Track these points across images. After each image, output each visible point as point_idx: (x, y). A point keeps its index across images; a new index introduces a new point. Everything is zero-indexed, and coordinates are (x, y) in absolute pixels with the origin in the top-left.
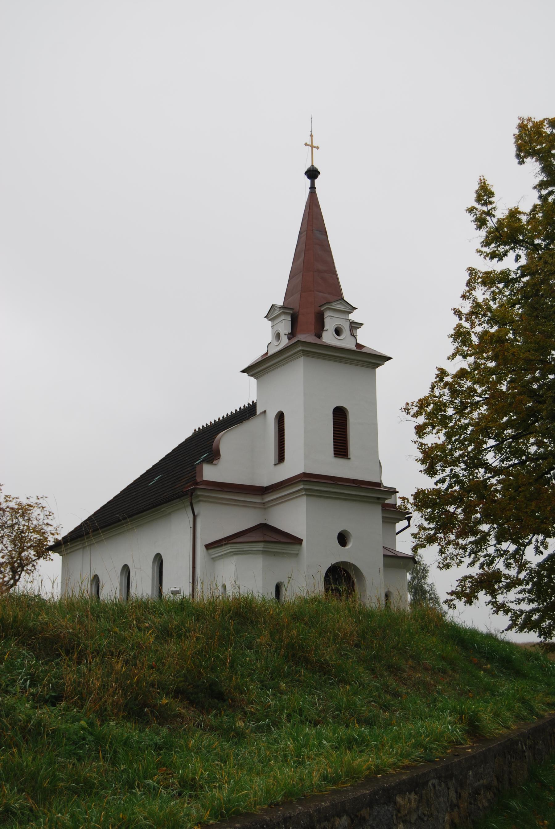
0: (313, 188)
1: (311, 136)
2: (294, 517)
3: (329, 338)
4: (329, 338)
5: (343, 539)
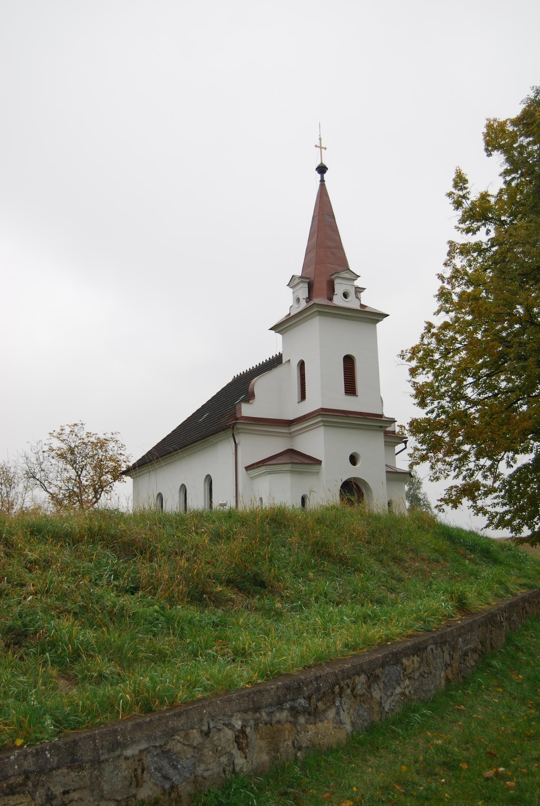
0: (322, 181)
1: (320, 139)
2: (314, 442)
3: (338, 300)
4: (338, 300)
5: (353, 460)
